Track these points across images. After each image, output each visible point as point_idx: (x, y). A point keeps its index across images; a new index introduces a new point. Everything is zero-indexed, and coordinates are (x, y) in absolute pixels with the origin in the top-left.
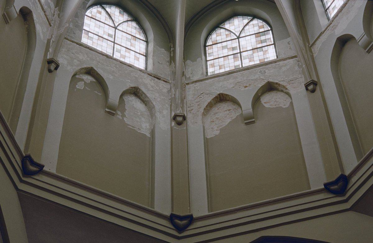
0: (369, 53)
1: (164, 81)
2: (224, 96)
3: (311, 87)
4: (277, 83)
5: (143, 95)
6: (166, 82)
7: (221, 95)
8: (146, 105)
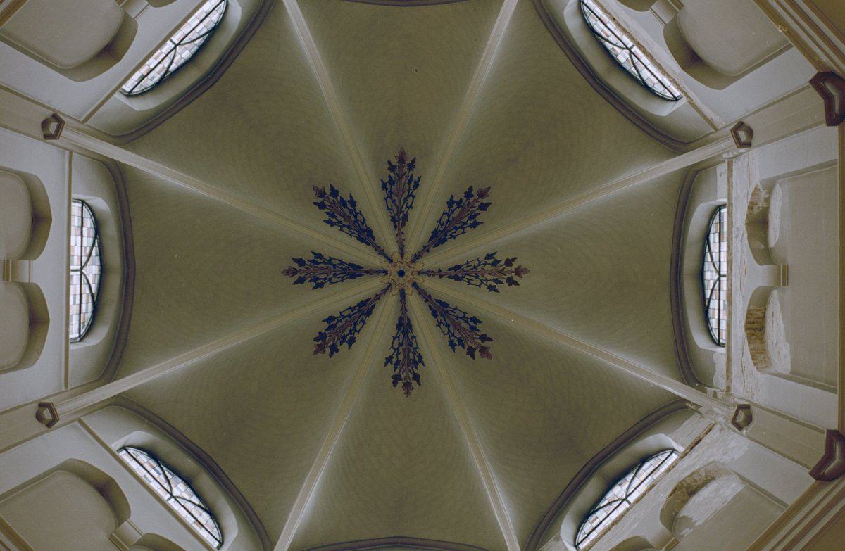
0: (683, 6)
1: (707, 433)
2: (753, 320)
4: (751, 208)
5: (695, 477)
6: (710, 430)
7: (749, 326)
8: (713, 479)
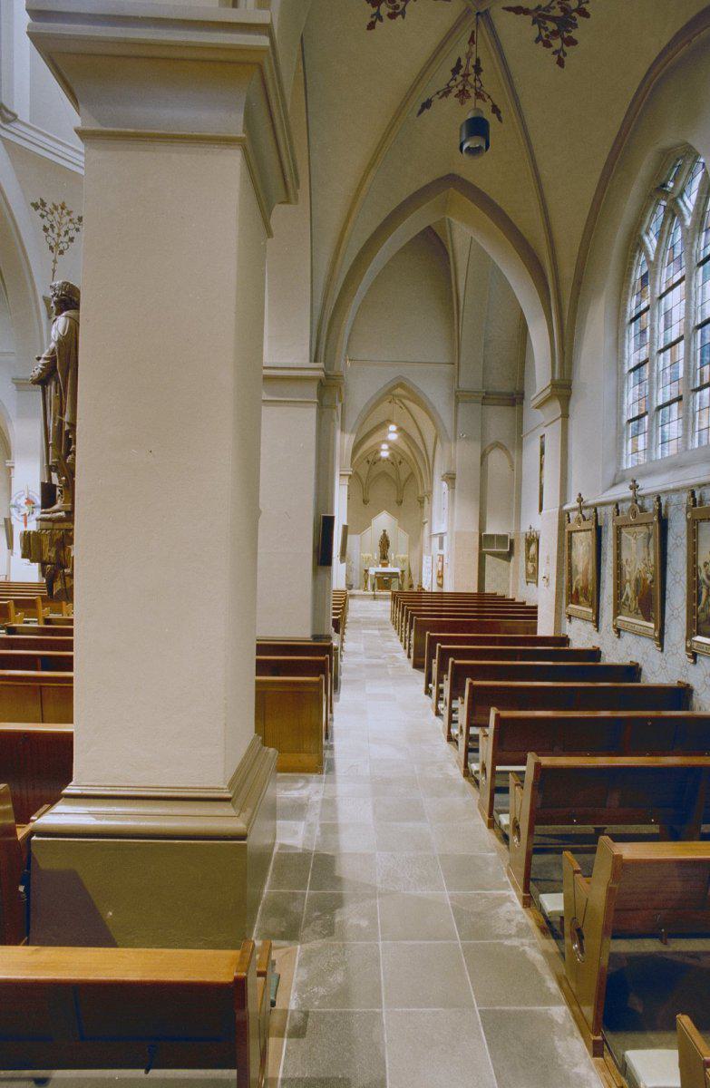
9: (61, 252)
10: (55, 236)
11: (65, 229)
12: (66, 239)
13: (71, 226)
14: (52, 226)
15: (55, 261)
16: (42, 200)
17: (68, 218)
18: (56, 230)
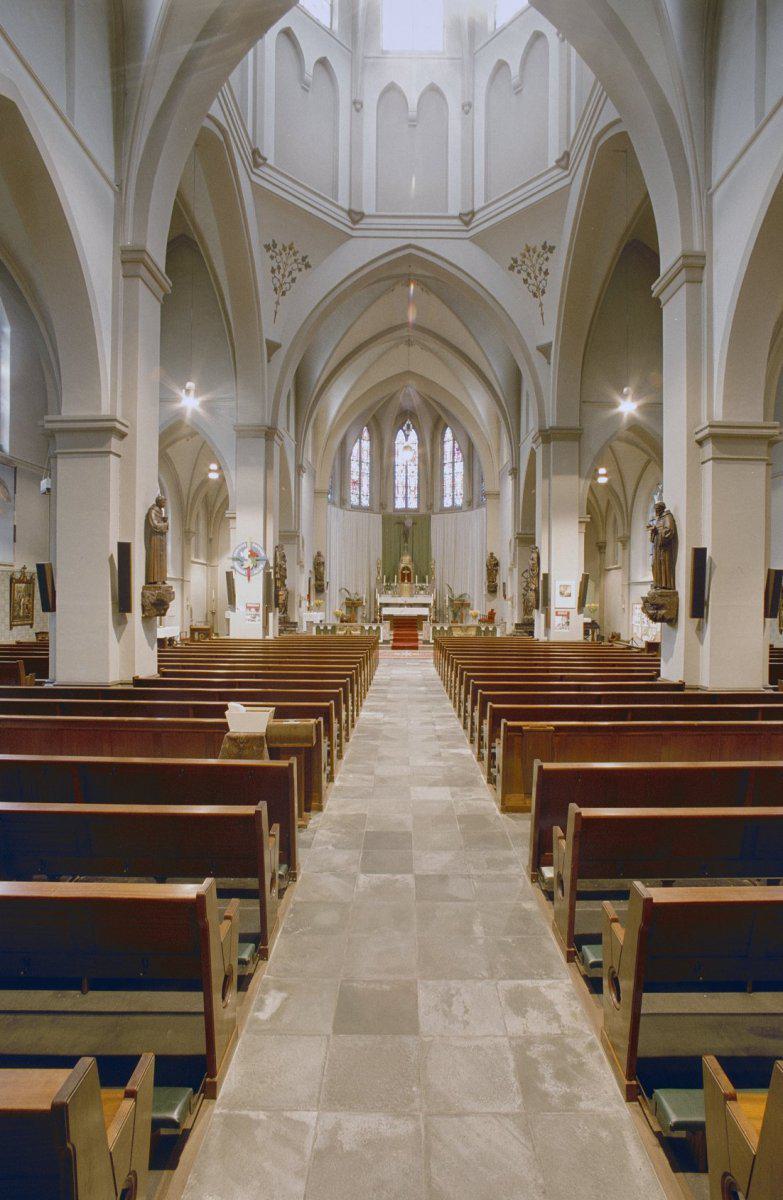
3: (467, 108)
9: (284, 294)
10: (280, 277)
11: (289, 269)
12: (289, 280)
13: (295, 266)
14: (279, 268)
15: (277, 303)
16: (274, 241)
17: (293, 258)
18: (282, 271)
